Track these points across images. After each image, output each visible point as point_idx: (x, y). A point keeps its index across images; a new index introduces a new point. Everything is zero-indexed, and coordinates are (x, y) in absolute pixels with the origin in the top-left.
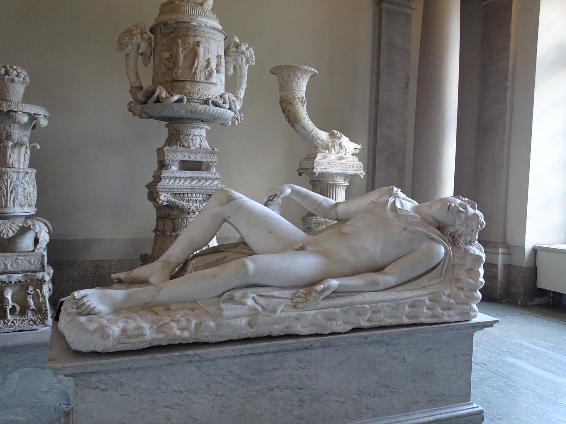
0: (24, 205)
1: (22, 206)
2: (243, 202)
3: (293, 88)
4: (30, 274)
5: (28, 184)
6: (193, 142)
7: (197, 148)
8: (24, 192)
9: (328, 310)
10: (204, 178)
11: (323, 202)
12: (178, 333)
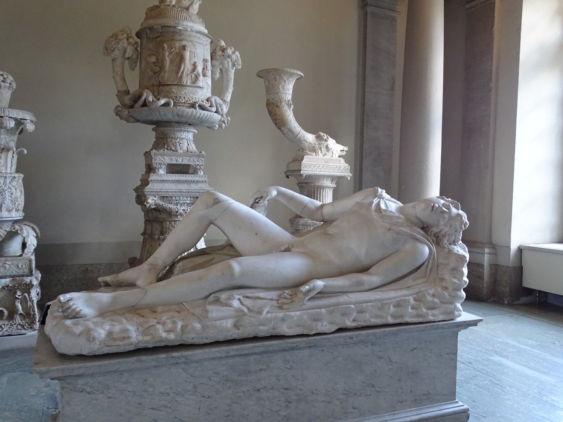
0: (11, 209)
1: (9, 211)
2: (229, 204)
3: (279, 91)
4: (18, 278)
5: (16, 189)
6: (180, 145)
7: (184, 151)
8: (11, 197)
9: (313, 311)
10: (191, 181)
11: (309, 204)
12: (164, 335)
